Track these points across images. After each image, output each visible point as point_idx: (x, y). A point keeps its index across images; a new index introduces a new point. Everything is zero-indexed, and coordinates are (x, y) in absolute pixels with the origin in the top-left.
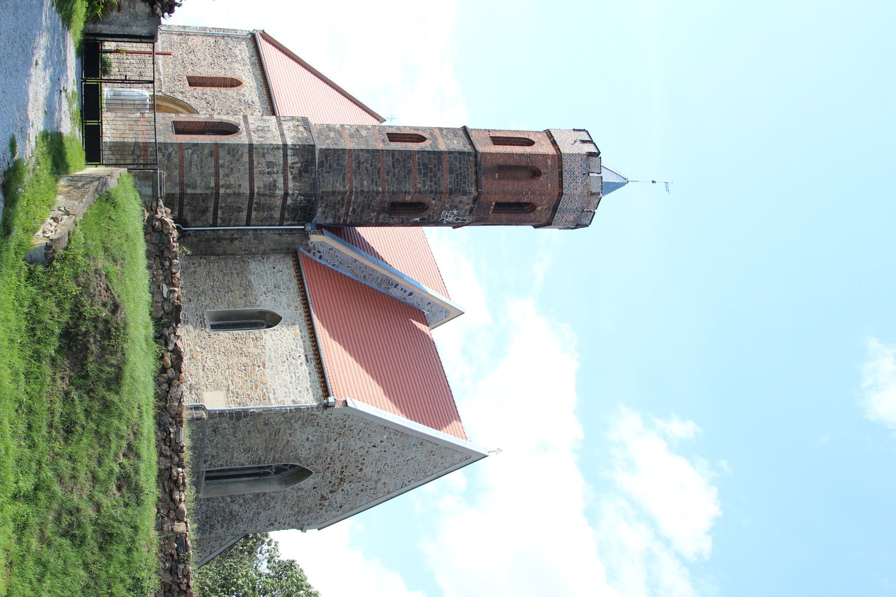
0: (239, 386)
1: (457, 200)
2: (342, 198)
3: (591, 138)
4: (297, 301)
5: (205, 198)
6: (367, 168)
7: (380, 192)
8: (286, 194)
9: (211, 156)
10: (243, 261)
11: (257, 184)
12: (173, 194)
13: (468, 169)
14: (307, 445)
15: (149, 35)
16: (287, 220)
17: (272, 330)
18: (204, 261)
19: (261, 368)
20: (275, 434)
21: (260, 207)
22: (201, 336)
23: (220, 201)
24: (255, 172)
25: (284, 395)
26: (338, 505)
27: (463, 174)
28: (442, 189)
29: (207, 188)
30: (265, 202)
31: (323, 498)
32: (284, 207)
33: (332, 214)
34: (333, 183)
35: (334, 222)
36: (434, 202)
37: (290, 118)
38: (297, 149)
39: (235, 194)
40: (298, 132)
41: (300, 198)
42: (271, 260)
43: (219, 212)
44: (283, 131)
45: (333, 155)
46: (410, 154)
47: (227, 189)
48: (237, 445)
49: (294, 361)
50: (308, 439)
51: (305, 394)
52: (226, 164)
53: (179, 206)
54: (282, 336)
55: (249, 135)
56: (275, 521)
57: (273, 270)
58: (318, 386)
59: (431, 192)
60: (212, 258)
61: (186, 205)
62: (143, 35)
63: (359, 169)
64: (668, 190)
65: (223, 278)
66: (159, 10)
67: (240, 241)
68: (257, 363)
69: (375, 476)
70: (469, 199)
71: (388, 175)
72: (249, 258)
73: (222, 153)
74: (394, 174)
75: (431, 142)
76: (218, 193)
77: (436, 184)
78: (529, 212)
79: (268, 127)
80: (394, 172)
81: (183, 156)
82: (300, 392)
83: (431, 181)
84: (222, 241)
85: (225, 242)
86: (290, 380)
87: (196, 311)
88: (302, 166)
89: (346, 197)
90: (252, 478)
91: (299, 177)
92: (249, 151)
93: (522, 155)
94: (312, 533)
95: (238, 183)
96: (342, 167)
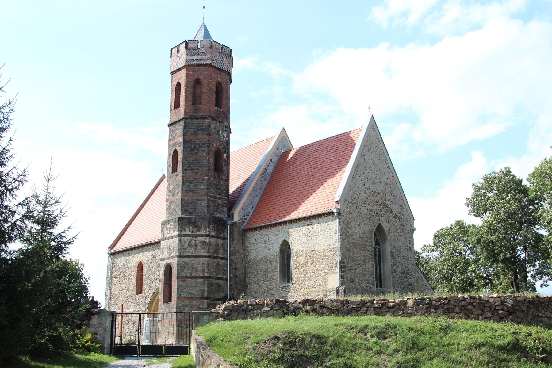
0: (325, 266)
1: (213, 131)
2: (212, 201)
6: (193, 186)
8: (209, 236)
9: (185, 280)
10: (249, 262)
11: (202, 253)
12: (208, 304)
14: (362, 226)
16: (224, 235)
18: (248, 286)
19: (314, 252)
21: (216, 251)
26: (400, 208)
29: (204, 283)
30: (213, 248)
32: (216, 237)
34: (202, 207)
36: (215, 145)
38: (181, 229)
39: (208, 267)
40: (170, 228)
42: (249, 245)
43: (219, 276)
45: (185, 206)
46: (185, 159)
47: (205, 271)
48: (361, 268)
49: (311, 233)
50: (359, 225)
51: (331, 226)
52: (190, 272)
55: (172, 257)
56: (408, 246)
58: (327, 218)
59: (209, 146)
61: (214, 296)
62: (111, 320)
63: (194, 191)
65: (259, 275)
66: (96, 310)
67: (237, 264)
69: (383, 185)
70: (213, 123)
71: (198, 173)
72: (248, 259)
73: (183, 274)
74: (197, 169)
75: (177, 146)
76: (207, 277)
78: (222, 86)
80: (196, 169)
82: (330, 229)
83: (202, 146)
85: (237, 273)
86: (322, 235)
88: (192, 226)
89: (211, 199)
90: (382, 259)
94: (416, 224)
95: (201, 265)
96: (192, 201)
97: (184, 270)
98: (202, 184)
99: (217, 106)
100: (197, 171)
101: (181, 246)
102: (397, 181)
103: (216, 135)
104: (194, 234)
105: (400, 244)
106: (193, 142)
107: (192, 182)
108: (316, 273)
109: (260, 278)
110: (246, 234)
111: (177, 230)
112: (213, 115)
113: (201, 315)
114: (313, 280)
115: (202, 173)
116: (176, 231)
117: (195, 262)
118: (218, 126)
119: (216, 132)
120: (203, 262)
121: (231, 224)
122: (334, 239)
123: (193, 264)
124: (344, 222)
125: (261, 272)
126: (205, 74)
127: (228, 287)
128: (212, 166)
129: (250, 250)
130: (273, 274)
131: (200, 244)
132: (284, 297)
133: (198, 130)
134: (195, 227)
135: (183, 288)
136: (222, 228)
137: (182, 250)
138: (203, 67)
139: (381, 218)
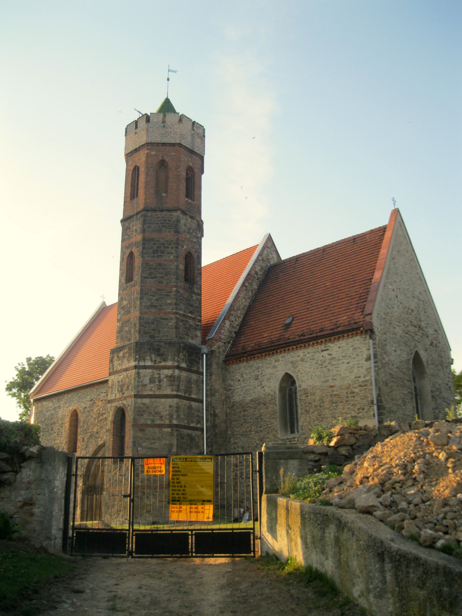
0: (352, 407)
1: (183, 228)
2: (182, 321)
4: (270, 360)
5: (181, 437)
6: (157, 300)
7: (177, 290)
8: (178, 367)
9: (143, 430)
10: (233, 406)
11: (168, 391)
13: (158, 218)
14: (399, 352)
15: (66, 464)
16: (198, 368)
18: (232, 439)
19: (334, 389)
20: (393, 378)
21: (188, 390)
23: (183, 424)
24: (158, 393)
25: (360, 369)
26: (435, 333)
29: (171, 434)
30: (184, 386)
31: (431, 344)
32: (188, 370)
34: (169, 328)
35: (200, 330)
36: (185, 247)
37: (111, 364)
38: (139, 358)
39: (177, 411)
40: (124, 357)
41: (181, 356)
42: (232, 383)
43: (192, 425)
44: (123, 369)
45: (145, 327)
46: (145, 265)
47: (173, 418)
48: (401, 411)
49: (327, 362)
50: (395, 351)
51: (359, 350)
52: (151, 418)
54: (303, 372)
55: (126, 398)
56: (447, 385)
57: (241, 381)
58: (352, 340)
59: (177, 247)
60: (229, 432)
62: (66, 472)
63: (157, 306)
64: (175, 72)
65: (248, 423)
66: (34, 449)
67: (216, 409)
68: (329, 392)
69: (416, 300)
70: (183, 218)
71: (162, 282)
73: (142, 421)
74: (162, 277)
75: (134, 248)
76: (176, 426)
77: (170, 244)
78: (194, 172)
79: (118, 382)
80: (160, 277)
82: (357, 355)
83: (168, 248)
84: (216, 423)
88: (154, 353)
90: (419, 401)
92: (140, 398)
93: (147, 174)
94: (453, 355)
95: (168, 408)
96: (154, 320)
97: (142, 415)
99: (187, 195)
101: (139, 382)
102: (430, 297)
104: (156, 365)
105: (440, 382)
107: (155, 294)
110: (227, 367)
111: (133, 359)
112: (183, 208)
113: (280, 459)
115: (168, 283)
116: (132, 361)
117: (158, 404)
120: (170, 404)
122: (365, 368)
123: (156, 407)
124: (379, 344)
125: (251, 419)
128: (182, 274)
129: (234, 389)
130: (269, 422)
131: (165, 380)
133: (163, 226)
135: (141, 441)
136: (195, 358)
137: (140, 388)
138: (169, 146)
139: (417, 344)
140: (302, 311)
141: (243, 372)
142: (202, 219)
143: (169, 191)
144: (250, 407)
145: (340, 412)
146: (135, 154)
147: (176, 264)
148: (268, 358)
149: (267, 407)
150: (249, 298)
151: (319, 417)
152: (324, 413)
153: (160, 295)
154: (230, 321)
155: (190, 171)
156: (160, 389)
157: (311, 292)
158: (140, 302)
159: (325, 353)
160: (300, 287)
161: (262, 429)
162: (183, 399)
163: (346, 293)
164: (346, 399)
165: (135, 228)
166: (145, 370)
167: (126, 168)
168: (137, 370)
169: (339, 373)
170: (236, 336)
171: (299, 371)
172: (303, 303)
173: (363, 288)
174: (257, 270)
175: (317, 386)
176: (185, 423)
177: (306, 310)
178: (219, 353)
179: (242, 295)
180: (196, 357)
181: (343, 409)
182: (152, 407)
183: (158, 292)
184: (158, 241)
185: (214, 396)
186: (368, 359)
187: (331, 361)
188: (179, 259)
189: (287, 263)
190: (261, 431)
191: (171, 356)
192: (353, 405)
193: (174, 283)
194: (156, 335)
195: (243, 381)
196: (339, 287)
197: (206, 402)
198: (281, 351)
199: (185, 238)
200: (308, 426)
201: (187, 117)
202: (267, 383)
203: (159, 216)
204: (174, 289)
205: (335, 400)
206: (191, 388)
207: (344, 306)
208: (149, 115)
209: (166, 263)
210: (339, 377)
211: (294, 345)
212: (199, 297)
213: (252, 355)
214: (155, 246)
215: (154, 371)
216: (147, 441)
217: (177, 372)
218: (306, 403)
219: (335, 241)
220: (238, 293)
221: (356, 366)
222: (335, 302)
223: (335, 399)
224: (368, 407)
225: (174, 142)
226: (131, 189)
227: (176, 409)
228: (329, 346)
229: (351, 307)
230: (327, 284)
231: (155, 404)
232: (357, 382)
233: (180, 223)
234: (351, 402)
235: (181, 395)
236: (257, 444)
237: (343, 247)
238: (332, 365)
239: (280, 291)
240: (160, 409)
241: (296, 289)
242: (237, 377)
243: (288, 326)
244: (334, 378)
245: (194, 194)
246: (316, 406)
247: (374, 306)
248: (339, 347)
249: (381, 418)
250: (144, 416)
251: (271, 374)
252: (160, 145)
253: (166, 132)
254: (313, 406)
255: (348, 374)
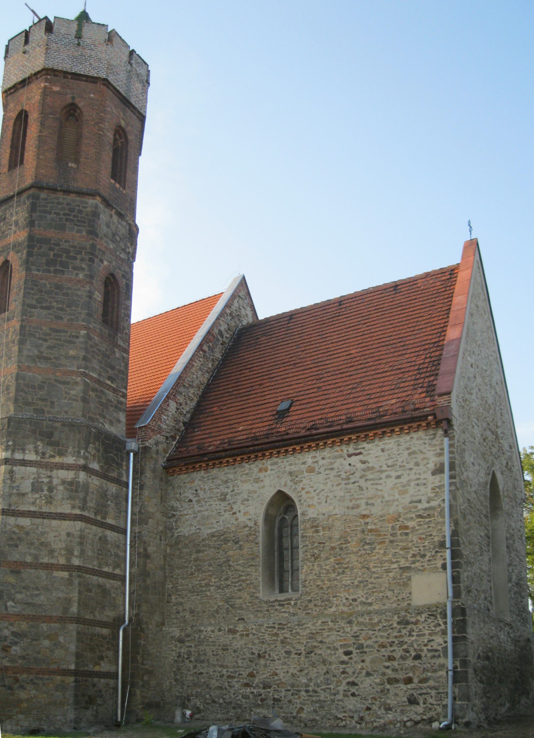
1: (104, 229)
3: (22, 32)
4: (250, 469)
5: (85, 588)
6: (49, 347)
7: (88, 334)
8: (85, 468)
9: (18, 572)
10: (177, 543)
11: (66, 509)
12: (78, 633)
13: (59, 203)
16: (120, 475)
17: (301, 504)
18: (173, 597)
21: (101, 509)
22: (306, 606)
23: (91, 566)
25: (422, 488)
27: (67, 212)
28: (88, 244)
29: (70, 582)
30: (94, 502)
32: (103, 476)
33: (114, 411)
34: (70, 399)
35: (124, 411)
36: (105, 263)
38: (14, 445)
41: (91, 448)
43: (106, 569)
45: (26, 393)
47: (73, 554)
49: (358, 474)
52: (33, 551)
53: (95, 626)
54: (312, 490)
58: (408, 438)
59: (91, 260)
61: (94, 616)
63: (50, 359)
65: (204, 572)
68: (360, 526)
71: (61, 318)
72: (172, 536)
74: (62, 309)
75: (12, 253)
76: (79, 568)
80: (58, 309)
81: (18, 615)
82: (417, 464)
83: (75, 258)
85: (149, 565)
86: (393, 479)
87: (261, 611)
88: (42, 440)
89: (92, 384)
91: (58, 446)
92: (13, 516)
93: (42, 124)
96: (45, 383)
97: (17, 546)
98: (72, 346)
100: (61, 313)
101: (12, 487)
103: (110, 242)
106: (54, 244)
107: (48, 338)
108: (374, 570)
109: (206, 581)
110: (170, 478)
114: (365, 586)
115: (72, 320)
117: (47, 530)
118: (114, 224)
119: (110, 235)
121: (136, 449)
122: (430, 486)
123: (43, 533)
125: (210, 565)
126: (91, 99)
127: (125, 598)
129: (181, 515)
130: (242, 571)
131: (61, 488)
132: (277, 626)
133: (67, 220)
134: (51, 444)
135: (13, 591)
137: (14, 498)
138: (86, 81)
140: (307, 392)
141: (198, 488)
142: (137, 222)
143: (82, 160)
144: (209, 546)
145: (378, 559)
146: (21, 91)
147: (88, 288)
148: (247, 465)
149: (241, 546)
150: (207, 372)
151: (337, 566)
152: (347, 560)
153: (56, 340)
154: (177, 403)
155: (120, 136)
156: (51, 503)
157: (323, 363)
158: (19, 348)
159: (354, 460)
160: (301, 357)
161: (229, 582)
162: (92, 524)
163: (391, 364)
164: (392, 538)
165: (14, 218)
166: (23, 468)
167: (4, 115)
168: (9, 467)
169: (379, 493)
170: (186, 429)
171: (303, 489)
172: (309, 379)
173: (423, 357)
174: (222, 329)
175: (336, 515)
176: (94, 565)
177: (315, 390)
178: (157, 452)
179: (197, 364)
180: (117, 455)
181: (385, 554)
182: (34, 533)
183: (53, 334)
184: (58, 244)
185: (147, 524)
186: (439, 470)
187: (365, 473)
188: (94, 282)
189: (272, 323)
190: (227, 586)
191: (74, 448)
192: (403, 549)
193: (83, 321)
194: (46, 409)
195: (198, 501)
196: (374, 355)
197: (131, 532)
198: (271, 453)
199: (106, 248)
200: (315, 580)
201: (120, 38)
202: (242, 507)
203: (61, 200)
204: (83, 332)
205: (370, 539)
206: (106, 506)
207: (390, 383)
208: (52, 20)
209: (70, 285)
210: (379, 501)
211: (297, 444)
212: (125, 355)
213: (217, 459)
214: (52, 253)
215: (41, 470)
216: (23, 590)
217: (82, 476)
218: (314, 542)
219: (359, 289)
220: (191, 360)
221: (413, 483)
222: (370, 378)
223: (369, 538)
224: (433, 553)
225: (95, 75)
226: (11, 152)
227: (78, 540)
228: (364, 448)
229: (402, 385)
230: (352, 352)
231: (40, 529)
232: (413, 510)
233: (99, 219)
234: (401, 544)
235: (88, 517)
236: (219, 606)
237: (375, 297)
238: (366, 480)
239: (263, 363)
240: (51, 537)
241: (294, 358)
242: (186, 494)
243: (282, 414)
244: (370, 502)
245: (125, 177)
246: (333, 548)
247: (453, 380)
248: (383, 450)
249: (458, 572)
250: (20, 547)
251: (250, 492)
252: (69, 77)
253: (82, 55)
254: (328, 548)
255: (397, 496)
